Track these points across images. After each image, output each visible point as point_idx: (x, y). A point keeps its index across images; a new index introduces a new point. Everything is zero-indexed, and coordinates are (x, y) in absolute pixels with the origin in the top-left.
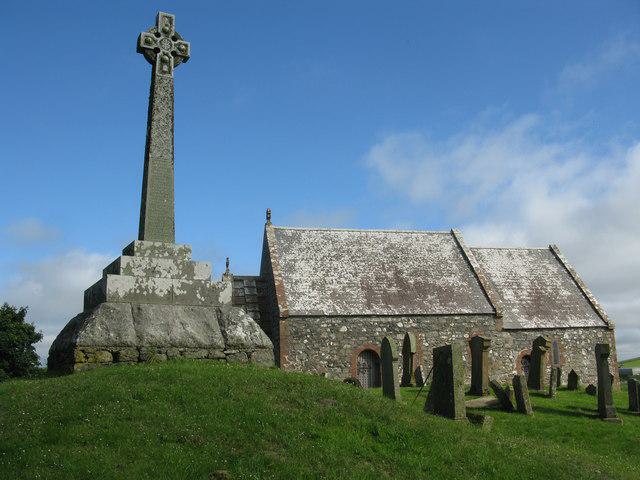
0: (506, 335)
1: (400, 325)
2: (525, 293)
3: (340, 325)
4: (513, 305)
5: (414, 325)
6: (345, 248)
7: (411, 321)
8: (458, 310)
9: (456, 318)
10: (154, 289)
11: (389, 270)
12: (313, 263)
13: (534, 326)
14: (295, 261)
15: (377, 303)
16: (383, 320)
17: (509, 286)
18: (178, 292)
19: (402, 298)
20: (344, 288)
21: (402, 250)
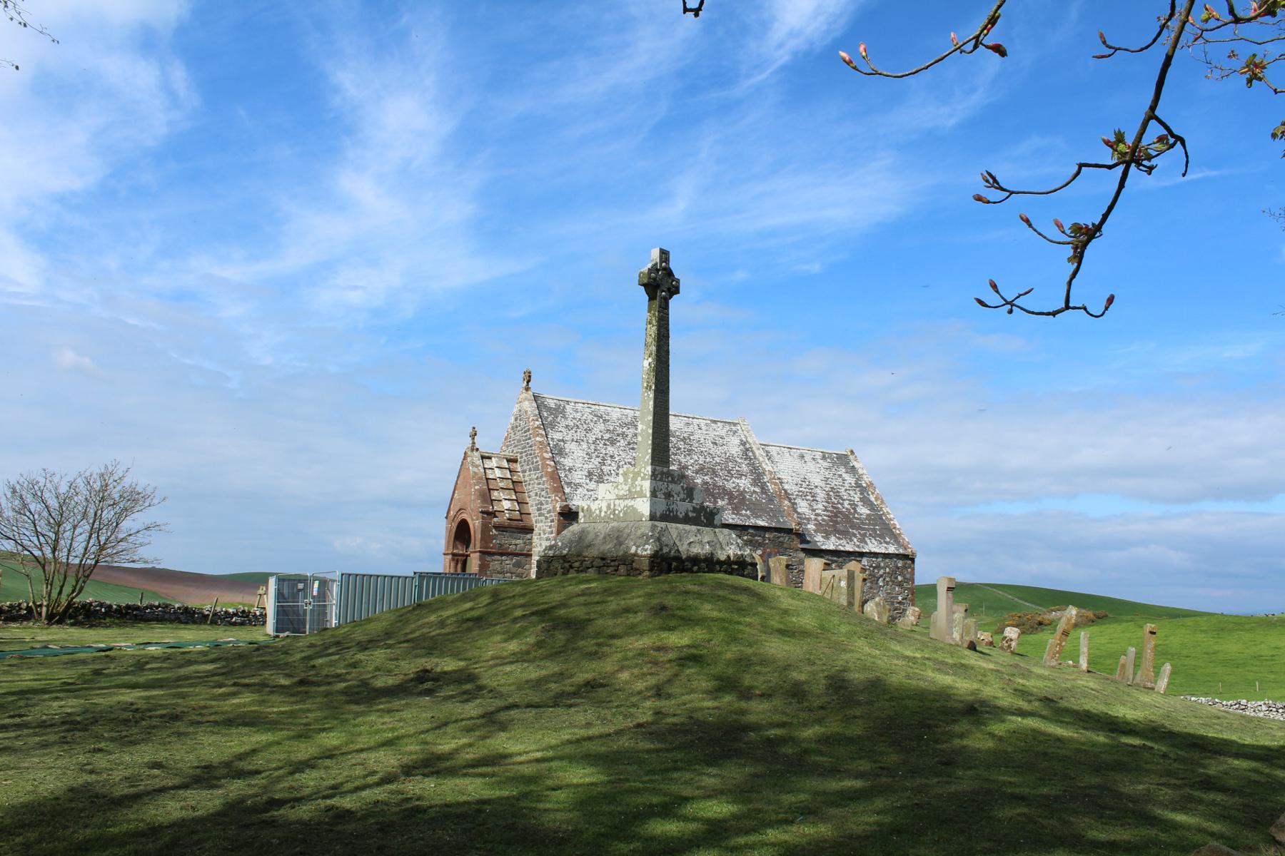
2: (820, 506)
6: (620, 430)
8: (752, 522)
9: (750, 531)
10: (677, 511)
12: (585, 446)
13: (832, 547)
14: (563, 441)
17: (803, 495)
18: (691, 514)
21: (684, 440)
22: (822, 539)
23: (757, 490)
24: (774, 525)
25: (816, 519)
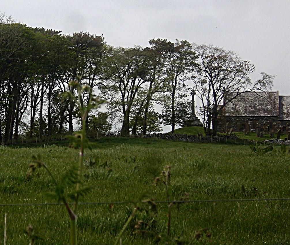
0: (279, 122)
1: (251, 119)
3: (237, 119)
4: (285, 114)
5: (255, 119)
7: (254, 118)
11: (253, 104)
15: (246, 113)
16: (247, 117)
19: (253, 112)
20: (240, 110)
22: (286, 118)
23: (272, 108)
24: (272, 116)
25: (287, 114)
